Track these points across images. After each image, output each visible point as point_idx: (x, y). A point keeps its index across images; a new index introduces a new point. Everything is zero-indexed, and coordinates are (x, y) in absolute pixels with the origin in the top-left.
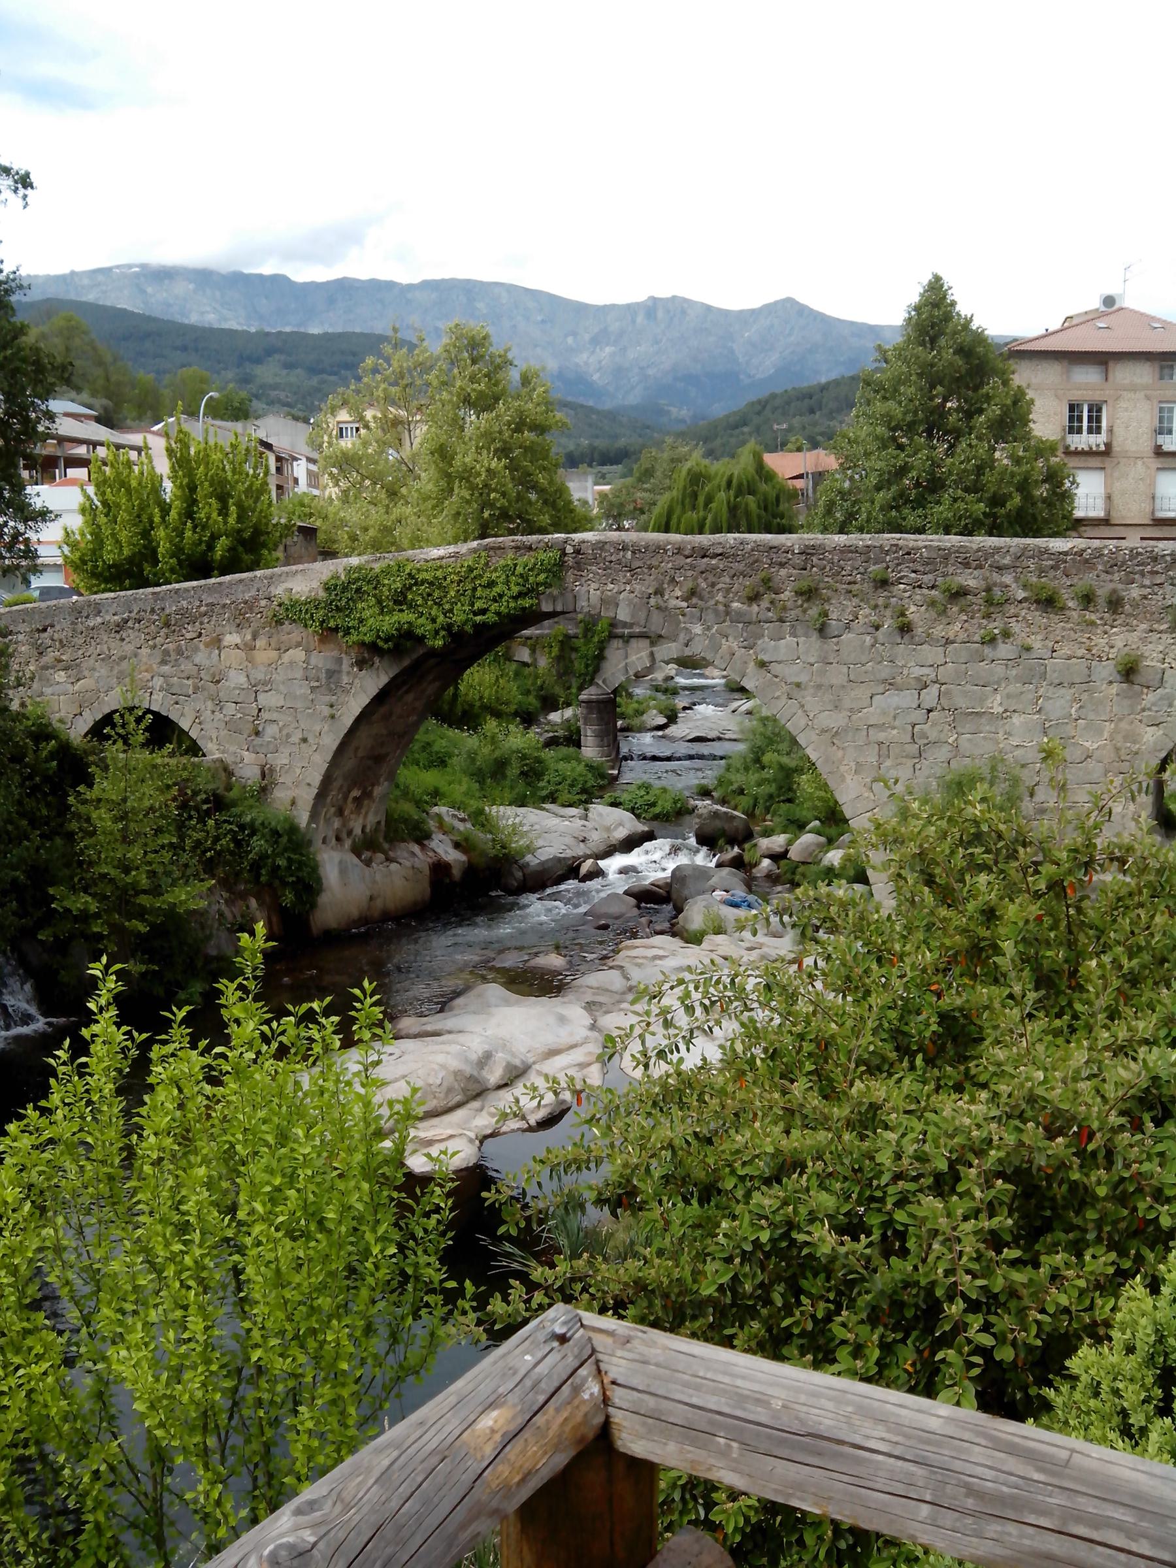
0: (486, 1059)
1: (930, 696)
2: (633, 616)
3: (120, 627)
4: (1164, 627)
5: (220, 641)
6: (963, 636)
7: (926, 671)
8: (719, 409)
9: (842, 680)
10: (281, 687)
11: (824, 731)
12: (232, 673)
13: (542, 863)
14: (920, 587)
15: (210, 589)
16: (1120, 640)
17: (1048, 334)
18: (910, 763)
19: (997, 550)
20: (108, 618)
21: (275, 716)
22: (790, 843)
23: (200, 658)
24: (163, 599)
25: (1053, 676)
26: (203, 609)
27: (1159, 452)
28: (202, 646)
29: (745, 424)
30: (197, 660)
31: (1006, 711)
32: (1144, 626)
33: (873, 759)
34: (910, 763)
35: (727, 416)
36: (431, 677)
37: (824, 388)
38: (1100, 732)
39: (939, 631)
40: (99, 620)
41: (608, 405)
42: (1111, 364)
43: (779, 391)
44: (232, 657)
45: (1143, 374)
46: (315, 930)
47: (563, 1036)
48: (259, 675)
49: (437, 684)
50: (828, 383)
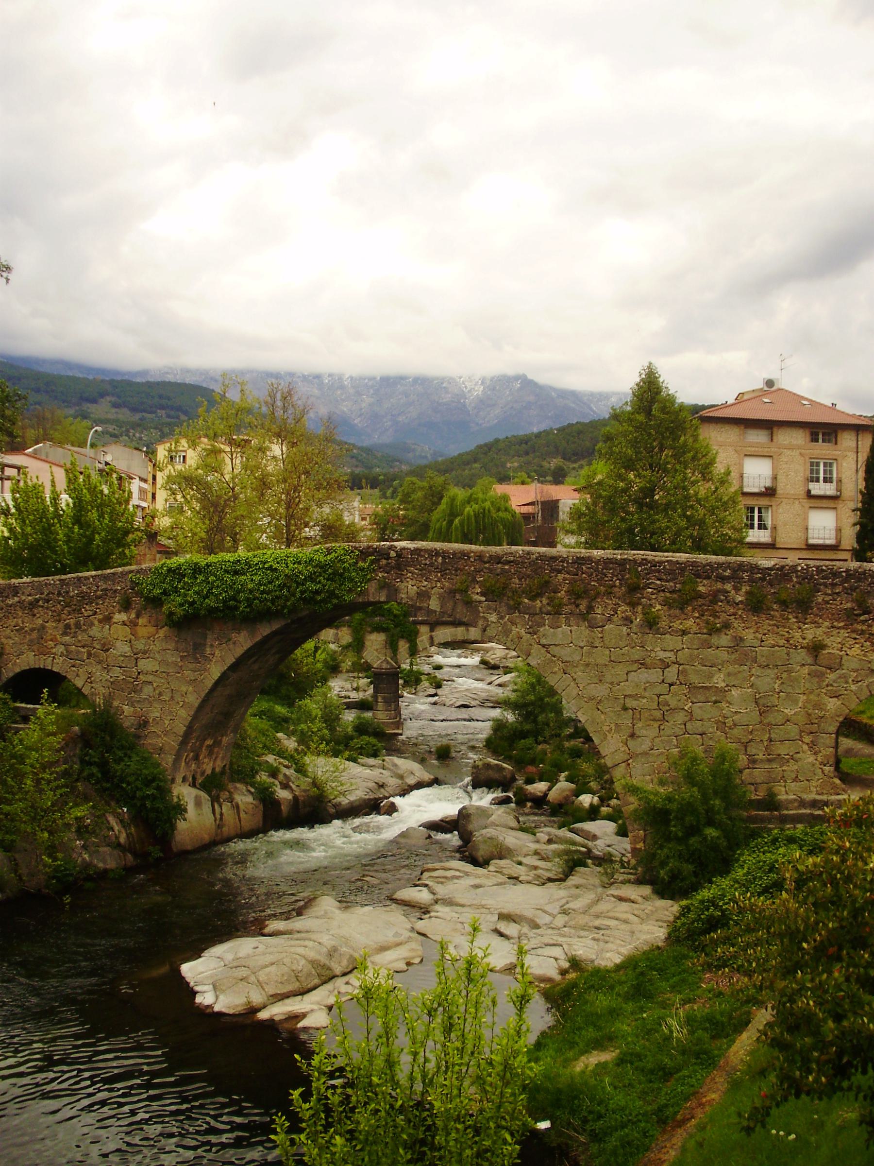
0: (332, 953)
1: (671, 674)
2: (442, 607)
3: (33, 605)
4: (842, 624)
5: (111, 618)
6: (695, 628)
7: (668, 654)
8: (454, 450)
9: (604, 660)
10: (157, 656)
11: (591, 699)
12: (118, 644)
13: (351, 803)
14: (663, 591)
15: (105, 578)
16: (811, 633)
17: (725, 406)
18: (656, 725)
19: (720, 565)
20: (23, 598)
21: (150, 678)
22: (550, 789)
23: (95, 631)
24: (68, 585)
25: (761, 660)
26: (99, 593)
27: (809, 495)
28: (96, 622)
29: (475, 461)
30: (91, 633)
31: (728, 685)
32: (827, 624)
33: (629, 722)
34: (656, 725)
35: (460, 455)
36: (273, 651)
37: (538, 435)
38: (796, 702)
39: (677, 625)
40: (16, 599)
41: (366, 443)
42: (775, 430)
43: (502, 437)
44: (124, 632)
45: (799, 438)
46: (175, 850)
47: (388, 936)
48: (140, 645)
49: (277, 656)
50: (540, 433)
